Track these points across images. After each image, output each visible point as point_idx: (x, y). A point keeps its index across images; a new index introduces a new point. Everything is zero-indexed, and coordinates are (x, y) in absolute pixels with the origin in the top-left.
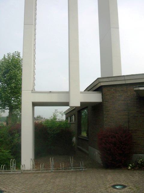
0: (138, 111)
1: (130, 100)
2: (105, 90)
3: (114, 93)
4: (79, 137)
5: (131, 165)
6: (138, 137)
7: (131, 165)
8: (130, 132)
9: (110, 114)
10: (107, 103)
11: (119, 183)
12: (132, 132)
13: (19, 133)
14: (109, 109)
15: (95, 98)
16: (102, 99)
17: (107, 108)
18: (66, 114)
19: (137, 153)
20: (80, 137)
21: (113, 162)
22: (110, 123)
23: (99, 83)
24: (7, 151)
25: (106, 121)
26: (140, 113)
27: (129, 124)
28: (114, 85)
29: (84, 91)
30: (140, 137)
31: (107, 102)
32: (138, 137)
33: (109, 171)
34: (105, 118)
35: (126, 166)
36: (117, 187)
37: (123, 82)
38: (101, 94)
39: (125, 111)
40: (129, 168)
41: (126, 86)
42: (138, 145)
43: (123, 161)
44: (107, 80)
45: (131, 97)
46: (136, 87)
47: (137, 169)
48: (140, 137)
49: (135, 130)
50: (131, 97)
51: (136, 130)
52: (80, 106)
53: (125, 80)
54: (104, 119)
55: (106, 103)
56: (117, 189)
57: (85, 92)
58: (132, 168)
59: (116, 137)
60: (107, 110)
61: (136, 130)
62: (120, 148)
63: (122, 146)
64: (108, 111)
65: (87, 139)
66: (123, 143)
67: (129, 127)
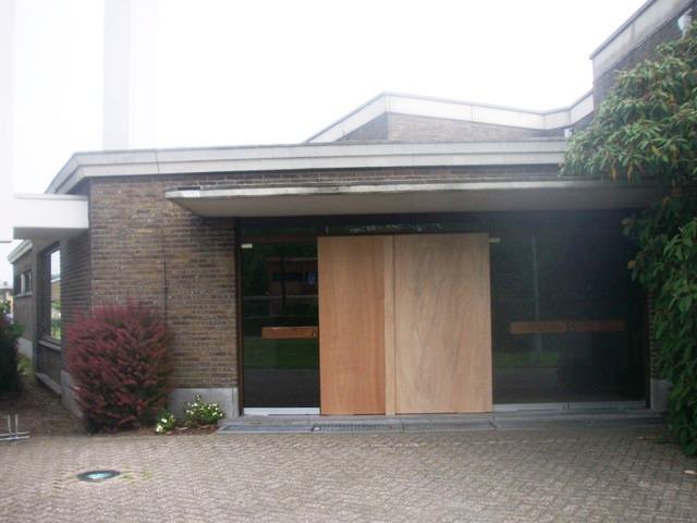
0: (192, 261)
1: (171, 226)
2: (96, 191)
3: (123, 202)
4: (42, 342)
5: (165, 421)
6: (194, 339)
7: (165, 421)
8: (170, 322)
9: (111, 268)
10: (103, 233)
11: (102, 468)
12: (174, 323)
13: (68, 385)
14: (105, 251)
15: (71, 215)
16: (90, 219)
17: (100, 248)
18: (13, 263)
19: (189, 387)
20: (49, 345)
21: (110, 414)
22: (110, 293)
23: (77, 168)
24: (103, 517)
25: (97, 288)
26: (200, 266)
27: (166, 298)
28: (137, 176)
29: (46, 192)
30: (198, 339)
31: (100, 230)
32: (194, 339)
33: (98, 439)
34: (96, 279)
35: (148, 423)
36: (94, 477)
37: (152, 170)
38: (86, 203)
39: (156, 257)
40: (159, 428)
41: (162, 181)
42: (191, 362)
43: (139, 408)
44: (113, 159)
45: (176, 216)
46: (172, 190)
47: (183, 432)
48: (198, 339)
49: (185, 318)
50: (176, 216)
51: (189, 317)
52: (321, 241)
53: (157, 163)
54: (93, 281)
55: (97, 233)
56: (95, 481)
57: (46, 196)
58: (166, 429)
59: (116, 337)
60: (102, 253)
61: (189, 317)
62: (130, 370)
63: (135, 363)
64: (106, 258)
65: (59, 348)
66: (137, 356)
67: (166, 309)
